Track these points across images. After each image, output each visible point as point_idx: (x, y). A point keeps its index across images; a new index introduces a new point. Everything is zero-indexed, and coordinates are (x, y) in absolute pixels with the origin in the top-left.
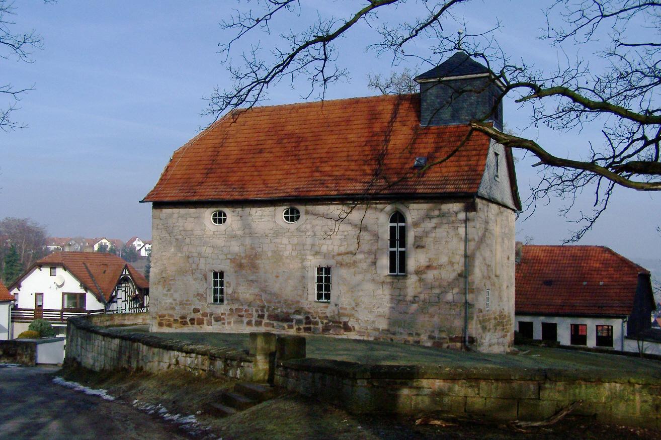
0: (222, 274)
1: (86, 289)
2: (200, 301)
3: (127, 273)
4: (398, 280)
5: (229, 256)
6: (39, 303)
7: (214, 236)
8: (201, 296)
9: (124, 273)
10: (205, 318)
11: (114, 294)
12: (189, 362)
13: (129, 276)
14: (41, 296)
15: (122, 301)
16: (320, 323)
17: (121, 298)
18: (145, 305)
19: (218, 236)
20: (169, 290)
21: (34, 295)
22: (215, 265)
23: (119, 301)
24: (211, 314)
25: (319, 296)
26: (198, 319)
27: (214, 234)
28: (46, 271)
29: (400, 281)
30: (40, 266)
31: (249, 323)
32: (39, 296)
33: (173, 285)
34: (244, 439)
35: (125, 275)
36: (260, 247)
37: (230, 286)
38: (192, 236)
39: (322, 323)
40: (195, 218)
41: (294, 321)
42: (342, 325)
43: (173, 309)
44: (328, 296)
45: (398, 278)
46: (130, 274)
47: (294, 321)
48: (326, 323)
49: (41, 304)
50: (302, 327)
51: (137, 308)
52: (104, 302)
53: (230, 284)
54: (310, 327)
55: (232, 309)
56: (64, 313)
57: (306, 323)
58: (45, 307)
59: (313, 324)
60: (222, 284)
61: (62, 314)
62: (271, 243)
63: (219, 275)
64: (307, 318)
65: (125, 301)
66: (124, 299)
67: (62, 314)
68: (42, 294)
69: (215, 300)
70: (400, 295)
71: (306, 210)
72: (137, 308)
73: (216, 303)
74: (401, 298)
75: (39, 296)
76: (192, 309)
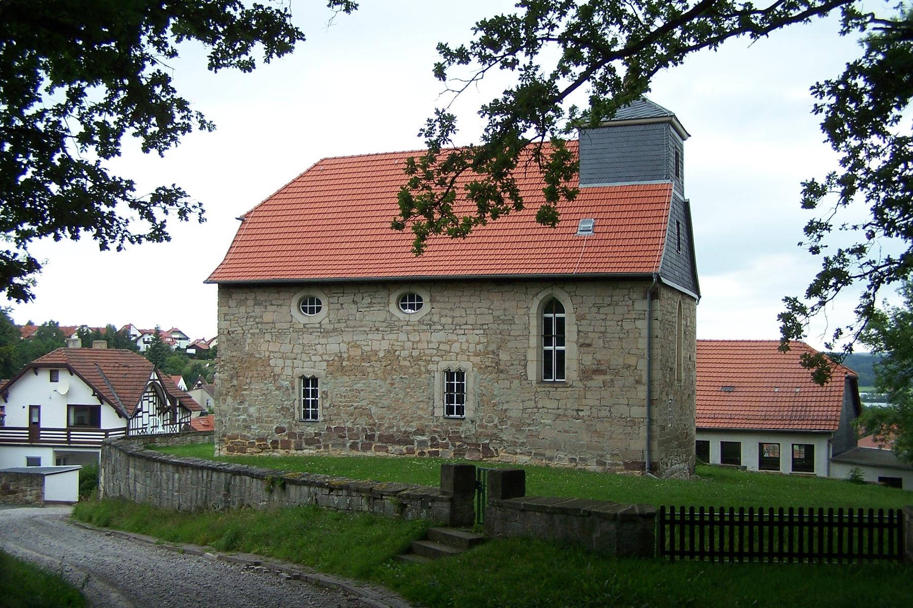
0: (315, 381)
1: (101, 398)
2: (285, 417)
3: (156, 378)
4: (556, 388)
5: (325, 357)
6: (35, 420)
7: (304, 330)
8: (284, 411)
9: (152, 378)
10: (293, 440)
11: (139, 407)
12: (336, 502)
13: (158, 382)
14: (37, 410)
15: (149, 416)
16: (450, 446)
17: (148, 412)
18: (178, 422)
19: (311, 330)
20: (242, 402)
21: (27, 409)
22: (305, 369)
23: (146, 415)
24: (301, 435)
25: (450, 410)
26: (283, 441)
27: (304, 327)
28: (44, 376)
29: (559, 389)
30: (36, 369)
31: (354, 446)
32: (34, 410)
33: (247, 395)
34: (606, 607)
35: (154, 380)
36: (368, 345)
37: (327, 397)
38: (273, 331)
39: (454, 445)
40: (278, 306)
41: (416, 444)
42: (481, 448)
43: (247, 427)
44: (460, 410)
45: (556, 385)
46: (159, 379)
47: (416, 444)
48: (459, 446)
49: (37, 421)
50: (426, 451)
51: (167, 425)
52: (126, 417)
53: (327, 394)
54: (438, 451)
55: (330, 428)
56: (72, 433)
57: (432, 446)
58: (42, 426)
59: (442, 447)
60: (315, 393)
61: (69, 435)
62: (383, 339)
63: (310, 382)
64: (433, 439)
65: (153, 415)
66: (151, 413)
67: (69, 435)
68: (38, 407)
69: (306, 415)
70: (558, 409)
71: (851, 345)
72: (167, 425)
73: (307, 420)
74: (560, 412)
75: (34, 410)
76: (275, 427)
